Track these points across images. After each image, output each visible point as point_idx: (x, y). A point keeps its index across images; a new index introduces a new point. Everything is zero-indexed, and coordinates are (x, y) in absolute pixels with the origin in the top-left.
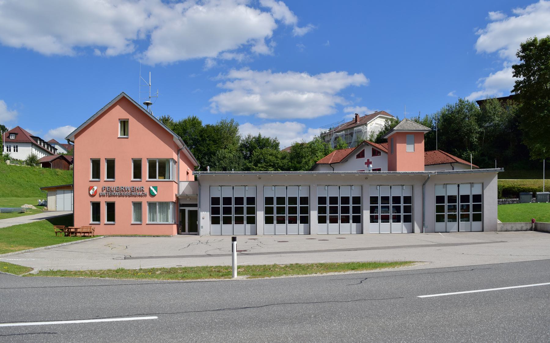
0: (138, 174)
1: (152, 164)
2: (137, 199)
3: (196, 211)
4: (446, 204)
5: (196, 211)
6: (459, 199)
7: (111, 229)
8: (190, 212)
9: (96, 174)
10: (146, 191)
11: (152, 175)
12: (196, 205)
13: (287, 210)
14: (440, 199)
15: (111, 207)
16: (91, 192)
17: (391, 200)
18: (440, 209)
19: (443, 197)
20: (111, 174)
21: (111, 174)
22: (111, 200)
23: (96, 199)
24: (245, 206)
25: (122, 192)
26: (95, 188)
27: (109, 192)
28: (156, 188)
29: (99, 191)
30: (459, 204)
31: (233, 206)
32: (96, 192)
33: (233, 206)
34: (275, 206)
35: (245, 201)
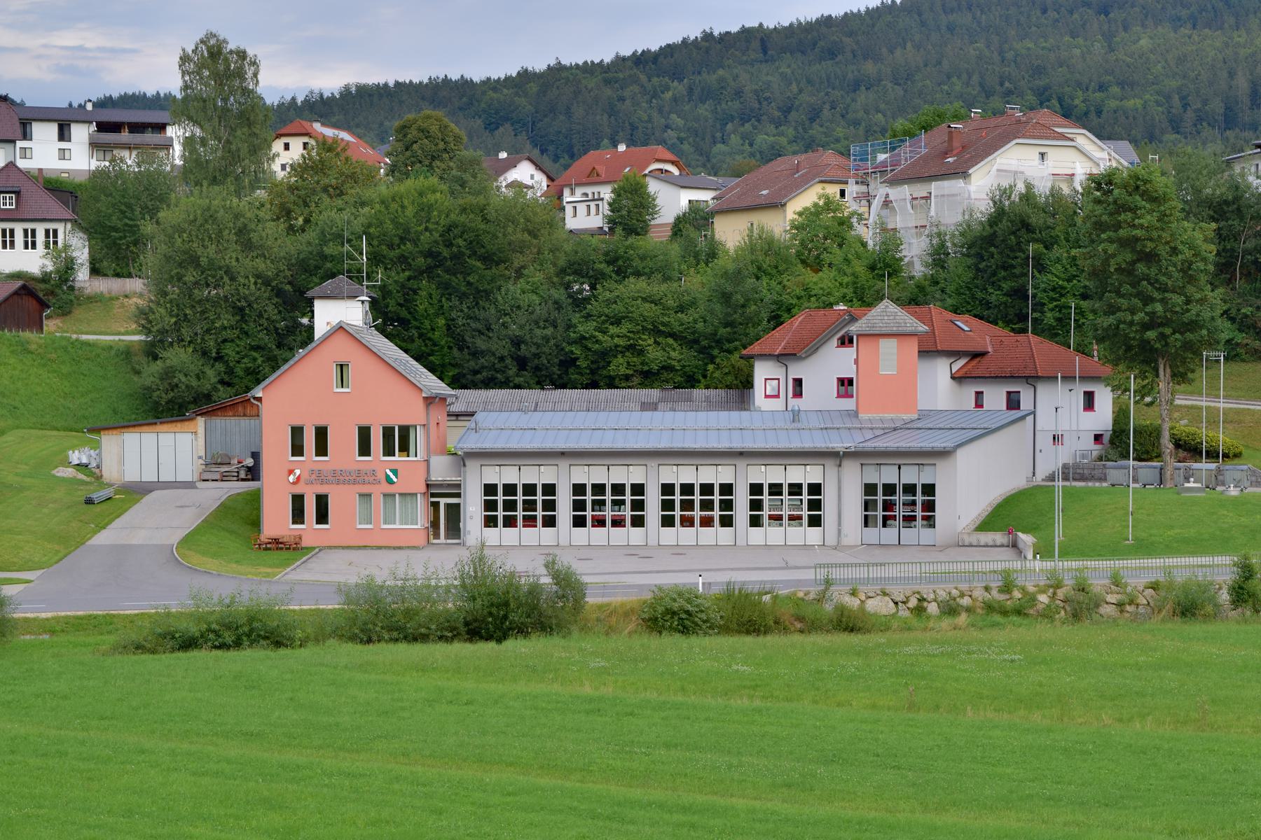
0: (365, 449)
1: (388, 432)
2: (365, 489)
3: (458, 505)
4: (677, 497)
5: (458, 505)
6: (900, 490)
7: (926, 535)
8: (448, 506)
9: (297, 450)
10: (381, 477)
11: (389, 451)
12: (458, 495)
13: (697, 505)
14: (490, 489)
15: (322, 501)
16: (291, 478)
17: (608, 490)
18: (490, 506)
19: (603, 486)
20: (322, 449)
21: (322, 449)
22: (322, 490)
23: (298, 490)
24: (539, 498)
25: (339, 478)
26: (298, 472)
27: (320, 477)
28: (395, 472)
29: (305, 477)
30: (899, 498)
31: (520, 498)
32: (299, 478)
33: (520, 498)
34: (500, 498)
35: (589, 490)
